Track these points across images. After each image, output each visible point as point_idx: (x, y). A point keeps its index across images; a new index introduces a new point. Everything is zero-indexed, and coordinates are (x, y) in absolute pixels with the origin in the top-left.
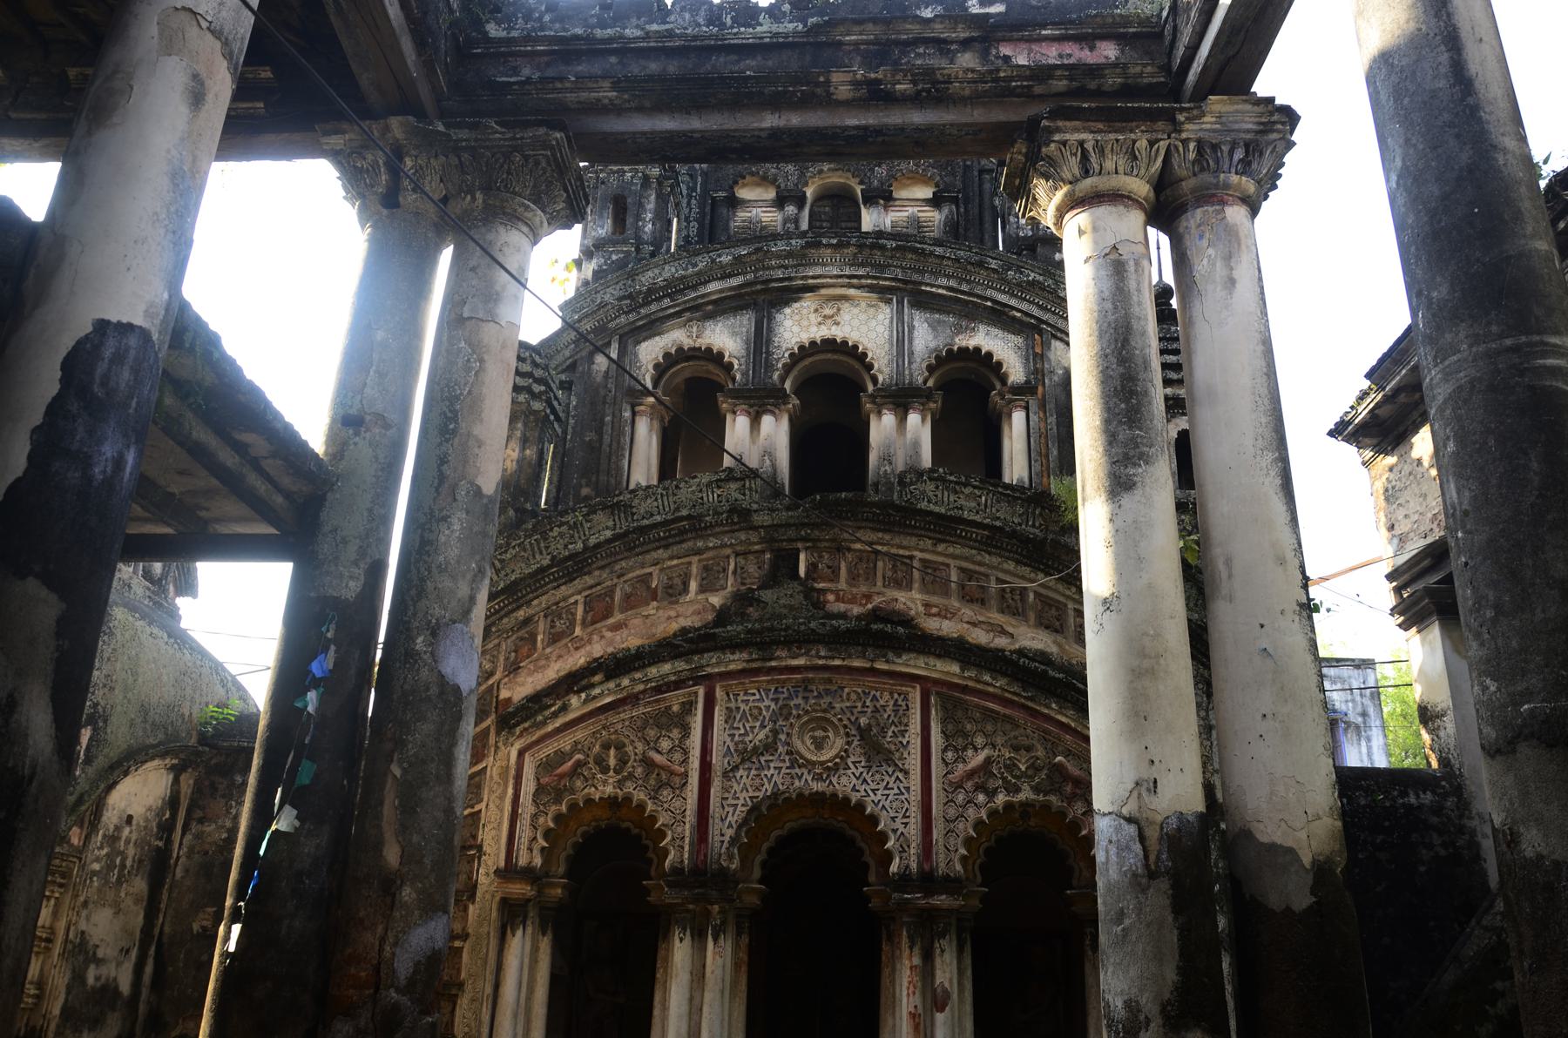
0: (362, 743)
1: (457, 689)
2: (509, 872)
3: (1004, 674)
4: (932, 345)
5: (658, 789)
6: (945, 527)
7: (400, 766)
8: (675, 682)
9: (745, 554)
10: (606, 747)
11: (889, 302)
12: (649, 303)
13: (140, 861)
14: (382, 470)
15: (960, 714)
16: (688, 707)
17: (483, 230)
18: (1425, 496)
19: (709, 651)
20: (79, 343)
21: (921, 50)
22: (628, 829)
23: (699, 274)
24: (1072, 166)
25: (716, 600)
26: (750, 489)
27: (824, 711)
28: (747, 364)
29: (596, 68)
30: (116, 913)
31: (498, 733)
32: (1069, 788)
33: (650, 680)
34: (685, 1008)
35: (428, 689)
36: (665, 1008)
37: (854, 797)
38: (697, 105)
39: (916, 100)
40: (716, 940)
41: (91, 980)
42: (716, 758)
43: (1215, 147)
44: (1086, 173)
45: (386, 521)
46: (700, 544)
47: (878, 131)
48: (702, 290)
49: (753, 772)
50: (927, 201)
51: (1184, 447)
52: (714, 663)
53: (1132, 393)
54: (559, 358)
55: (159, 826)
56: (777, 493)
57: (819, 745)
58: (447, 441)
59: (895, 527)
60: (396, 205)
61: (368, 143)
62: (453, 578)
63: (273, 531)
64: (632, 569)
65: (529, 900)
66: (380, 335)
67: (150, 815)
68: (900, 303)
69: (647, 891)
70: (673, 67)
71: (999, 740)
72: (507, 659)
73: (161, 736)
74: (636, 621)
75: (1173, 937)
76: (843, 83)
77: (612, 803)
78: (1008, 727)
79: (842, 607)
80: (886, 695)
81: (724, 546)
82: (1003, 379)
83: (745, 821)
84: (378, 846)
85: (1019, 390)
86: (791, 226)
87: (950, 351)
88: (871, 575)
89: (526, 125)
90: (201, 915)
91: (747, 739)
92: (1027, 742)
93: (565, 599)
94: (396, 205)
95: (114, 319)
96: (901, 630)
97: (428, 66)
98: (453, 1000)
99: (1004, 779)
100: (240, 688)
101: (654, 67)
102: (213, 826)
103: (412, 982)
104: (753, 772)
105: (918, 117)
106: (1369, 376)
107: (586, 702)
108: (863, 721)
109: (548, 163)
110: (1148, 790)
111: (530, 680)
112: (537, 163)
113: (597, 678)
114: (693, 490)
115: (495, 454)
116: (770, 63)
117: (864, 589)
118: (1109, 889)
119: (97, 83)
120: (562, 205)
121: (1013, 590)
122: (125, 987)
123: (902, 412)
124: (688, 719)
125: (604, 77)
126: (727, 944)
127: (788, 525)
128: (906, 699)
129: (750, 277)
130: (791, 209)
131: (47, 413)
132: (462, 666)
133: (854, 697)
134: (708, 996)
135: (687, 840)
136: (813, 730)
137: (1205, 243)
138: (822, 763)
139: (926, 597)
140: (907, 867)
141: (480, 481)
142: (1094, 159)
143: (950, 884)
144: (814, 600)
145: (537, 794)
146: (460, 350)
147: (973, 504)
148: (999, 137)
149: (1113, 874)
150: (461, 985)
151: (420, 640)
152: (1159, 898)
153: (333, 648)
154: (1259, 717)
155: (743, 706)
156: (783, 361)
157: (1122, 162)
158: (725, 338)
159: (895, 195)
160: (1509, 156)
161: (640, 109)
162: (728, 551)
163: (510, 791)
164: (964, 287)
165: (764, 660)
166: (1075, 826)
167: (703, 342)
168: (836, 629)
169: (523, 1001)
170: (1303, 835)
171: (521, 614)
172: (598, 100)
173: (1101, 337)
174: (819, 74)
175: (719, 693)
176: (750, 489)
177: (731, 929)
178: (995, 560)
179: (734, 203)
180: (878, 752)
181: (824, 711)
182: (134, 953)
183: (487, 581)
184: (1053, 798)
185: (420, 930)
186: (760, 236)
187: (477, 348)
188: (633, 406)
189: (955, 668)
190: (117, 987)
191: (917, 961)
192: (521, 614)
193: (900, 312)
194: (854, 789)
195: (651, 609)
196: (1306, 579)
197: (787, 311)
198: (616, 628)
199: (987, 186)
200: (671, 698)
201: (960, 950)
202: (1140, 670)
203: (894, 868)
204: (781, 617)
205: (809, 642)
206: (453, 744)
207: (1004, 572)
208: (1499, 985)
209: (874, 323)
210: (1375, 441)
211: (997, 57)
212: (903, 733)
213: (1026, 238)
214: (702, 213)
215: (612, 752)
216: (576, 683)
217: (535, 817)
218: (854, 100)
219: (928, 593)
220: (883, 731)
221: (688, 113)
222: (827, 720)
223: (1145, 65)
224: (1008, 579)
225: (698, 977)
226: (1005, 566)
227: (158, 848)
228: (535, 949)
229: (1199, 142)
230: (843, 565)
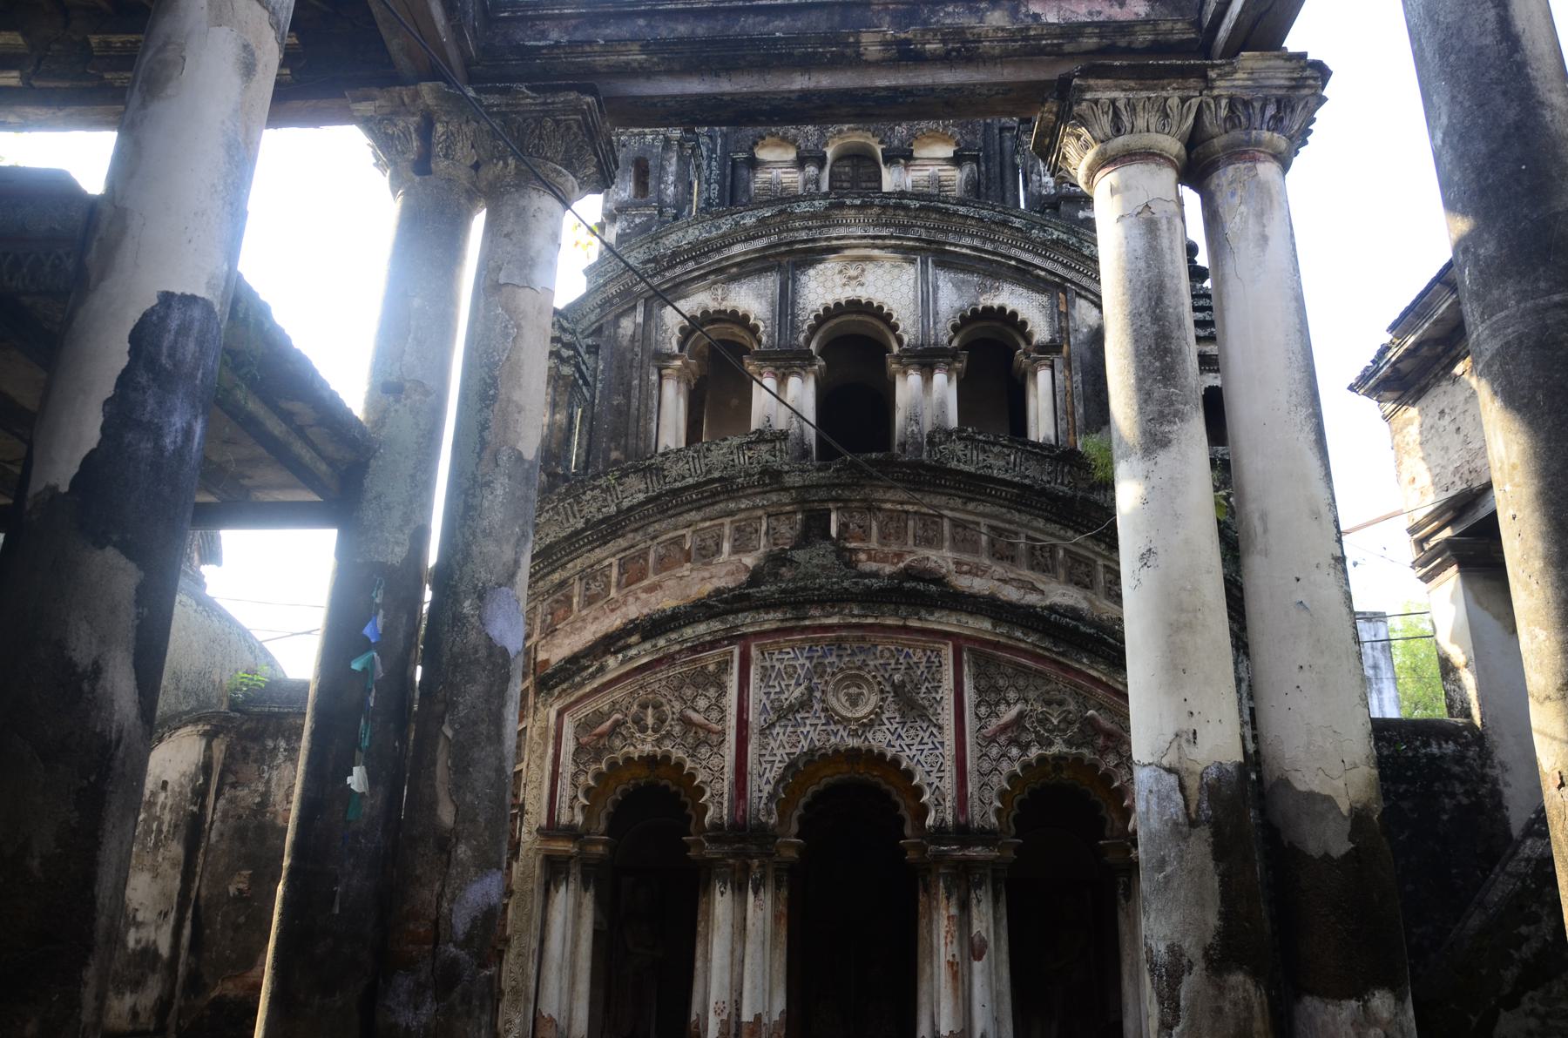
0: (411, 707)
1: (504, 651)
2: (551, 830)
3: (1036, 630)
4: (957, 305)
5: (695, 748)
6: (975, 486)
7: (452, 727)
8: (710, 642)
9: (776, 515)
10: (644, 706)
11: (913, 262)
12: (674, 267)
13: (176, 826)
14: (423, 436)
15: (992, 669)
16: (724, 666)
17: (516, 196)
18: (1446, 449)
19: (743, 610)
20: (145, 314)
21: (950, 9)
22: (666, 787)
23: (723, 236)
24: (1106, 122)
25: (749, 561)
26: (781, 451)
27: (859, 668)
28: (773, 326)
29: (624, 30)
30: (155, 877)
31: (537, 694)
32: (1100, 741)
33: (685, 641)
34: (727, 960)
35: (476, 652)
36: (707, 960)
37: (890, 753)
38: (727, 66)
39: (946, 60)
40: (756, 893)
41: (131, 943)
42: (753, 716)
43: (1247, 104)
44: (1118, 130)
45: (428, 486)
46: (732, 505)
47: (908, 92)
48: (727, 253)
49: (790, 729)
50: (948, 160)
51: (1214, 404)
52: (748, 622)
53: (1167, 351)
54: (585, 323)
55: (194, 791)
56: (805, 453)
57: (854, 702)
58: (487, 407)
59: (951, 487)
60: (429, 172)
61: (400, 109)
62: (498, 541)
63: (317, 499)
64: (666, 532)
65: (571, 857)
66: (417, 302)
67: (185, 781)
68: (924, 263)
69: (687, 847)
70: (702, 29)
71: (1032, 695)
72: (543, 621)
73: (193, 703)
74: (670, 583)
75: (1214, 883)
76: (873, 44)
77: (650, 761)
78: (1039, 682)
79: (874, 566)
80: (919, 653)
81: (755, 507)
82: (1028, 337)
83: (782, 778)
84: (432, 806)
85: (1044, 349)
86: (812, 187)
87: (974, 311)
88: (900, 534)
89: (557, 89)
90: (237, 878)
91: (783, 697)
92: (1059, 697)
93: (599, 562)
94: (429, 172)
95: (178, 291)
96: (933, 588)
97: (457, 30)
98: (500, 955)
99: (1037, 733)
100: (267, 654)
101: (682, 29)
102: (246, 791)
103: (469, 937)
104: (790, 729)
105: (949, 77)
106: (1392, 328)
107: (622, 663)
108: (897, 678)
109: (580, 127)
110: (1188, 741)
111: (567, 641)
112: (569, 128)
113: (634, 639)
114: (722, 454)
115: (532, 419)
116: (799, 24)
117: (895, 548)
118: (1151, 837)
119: (149, 54)
120: (593, 170)
121: (1042, 548)
122: (164, 949)
123: (927, 371)
124: (724, 678)
125: (633, 40)
126: (767, 897)
127: (818, 486)
128: (938, 655)
129: (774, 239)
130: (811, 170)
131: (117, 386)
132: (508, 626)
133: (887, 654)
134: (749, 948)
135: (726, 796)
136: (848, 687)
137: (1237, 200)
138: (857, 720)
139: (956, 555)
140: (943, 820)
141: (521, 446)
142: (1125, 117)
143: (985, 836)
144: (846, 558)
145: (577, 753)
146: (497, 316)
147: (1002, 463)
148: (1023, 98)
149: (1155, 823)
150: (507, 941)
151: (467, 603)
152: (1200, 846)
153: (381, 612)
154: (1296, 669)
155: (778, 665)
156: (809, 322)
157: (1154, 120)
158: (751, 300)
159: (915, 154)
160: (1556, 113)
161: (670, 72)
162: (760, 513)
163: (550, 751)
164: (988, 247)
165: (798, 619)
166: (1108, 778)
167: (728, 305)
168: (869, 588)
169: (567, 954)
170: (1340, 783)
171: (557, 577)
172: (628, 63)
173: (1133, 297)
174: (849, 35)
175: (754, 652)
176: (781, 451)
177: (770, 883)
178: (1025, 518)
179: (754, 164)
180: (912, 707)
181: (859, 668)
182: (172, 917)
183: (530, 545)
184: (1085, 751)
185: (476, 887)
186: (782, 199)
187: (512, 312)
188: (660, 370)
189: (987, 625)
190: (156, 950)
191: (953, 911)
192: (557, 577)
193: (924, 272)
194: (889, 745)
195: (685, 569)
196: (1339, 532)
197: (812, 272)
198: (651, 589)
199: (1008, 144)
200: (706, 658)
201: (996, 900)
202: (1177, 625)
203: (930, 821)
204: (814, 576)
205: (842, 600)
206: (502, 705)
207: (1033, 529)
208: (1524, 930)
209: (898, 284)
210: (1396, 395)
211: (1027, 15)
212: (936, 689)
213: (1048, 196)
214: (723, 175)
215: (650, 711)
216: (613, 644)
217: (575, 776)
218: (884, 60)
219: (958, 551)
220: (917, 687)
221: (717, 75)
222: (862, 677)
223: (1175, 22)
224: (1038, 536)
225: (740, 929)
226: (1035, 524)
227: (193, 813)
228: (578, 905)
229: (1232, 101)
230: (874, 524)
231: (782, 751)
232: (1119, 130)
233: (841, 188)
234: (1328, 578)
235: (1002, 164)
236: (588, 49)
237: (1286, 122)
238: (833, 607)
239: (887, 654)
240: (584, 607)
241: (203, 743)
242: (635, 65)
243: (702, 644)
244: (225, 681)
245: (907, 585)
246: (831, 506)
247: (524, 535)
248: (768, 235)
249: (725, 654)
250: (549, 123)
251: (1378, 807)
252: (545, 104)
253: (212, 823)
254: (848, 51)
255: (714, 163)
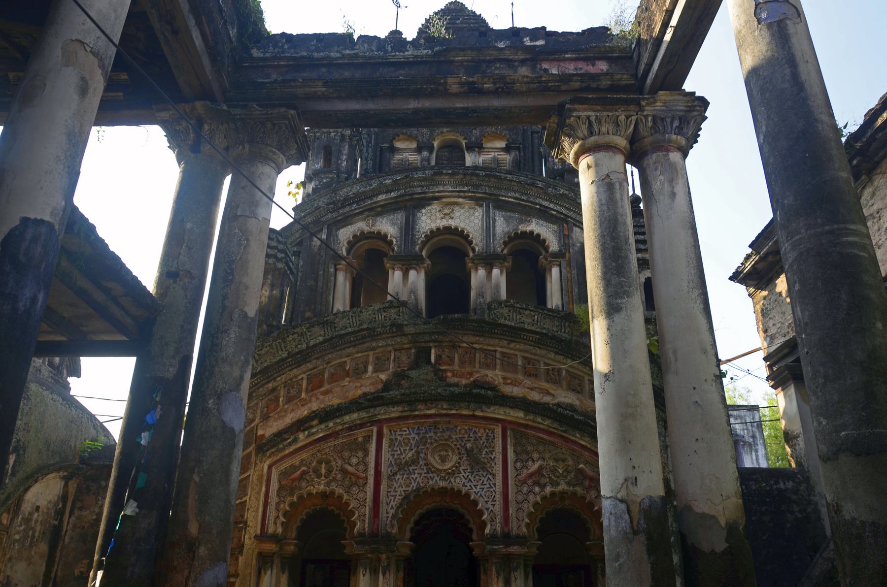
2: (262, 537)
3: (549, 418)
4: (506, 230)
6: (515, 333)
8: (360, 424)
10: (320, 462)
11: (481, 206)
13: (44, 533)
16: (367, 439)
18: (784, 313)
19: (379, 406)
21: (498, 65)
22: (333, 511)
23: (373, 190)
24: (583, 130)
25: (383, 377)
26: (403, 313)
27: (446, 440)
28: (401, 241)
30: (29, 564)
31: (256, 455)
32: (587, 483)
33: (345, 423)
39: (495, 93)
40: (384, 575)
43: (663, 120)
44: (591, 134)
46: (374, 344)
47: (474, 111)
48: (375, 200)
49: (405, 476)
50: (502, 149)
51: (648, 287)
52: (382, 413)
54: (293, 238)
56: (417, 313)
57: (443, 460)
58: (227, 286)
63: (124, 338)
68: (488, 206)
69: (344, 547)
70: (358, 74)
71: (547, 456)
72: (262, 412)
73: (57, 459)
74: (337, 389)
75: (647, 568)
76: (454, 83)
77: (324, 495)
79: (456, 380)
80: (482, 431)
81: (388, 345)
82: (546, 249)
83: (401, 505)
85: (555, 255)
86: (426, 163)
87: (516, 234)
91: (402, 457)
93: (296, 377)
94: (199, 151)
96: (490, 393)
99: (550, 478)
101: (347, 74)
102: (88, 512)
104: (405, 476)
105: (496, 103)
107: (308, 436)
108: (469, 445)
110: (632, 483)
111: (275, 424)
113: (315, 422)
114: (369, 313)
115: (255, 294)
116: (413, 72)
117: (468, 369)
121: (553, 369)
124: (367, 445)
126: (391, 577)
127: (424, 333)
128: (493, 432)
129: (402, 192)
130: (425, 154)
132: (236, 417)
133: (463, 431)
135: (367, 517)
136: (440, 451)
137: (658, 173)
138: (445, 470)
139: (503, 374)
141: (246, 309)
143: (520, 540)
144: (440, 376)
145: (279, 491)
147: (530, 320)
148: (543, 113)
149: (613, 532)
151: (211, 401)
152: (640, 545)
153: (159, 406)
154: (694, 440)
155: (399, 438)
158: (388, 226)
159: (484, 146)
161: (339, 98)
162: (390, 348)
163: (264, 489)
164: (524, 197)
166: (591, 505)
167: (375, 229)
170: (720, 508)
171: (270, 385)
172: (315, 92)
175: (385, 430)
176: (403, 313)
178: (543, 352)
179: (393, 150)
180: (477, 463)
181: (446, 440)
183: (250, 367)
186: (408, 168)
189: (521, 414)
192: (270, 385)
193: (488, 212)
194: (464, 485)
195: (346, 382)
197: (424, 211)
198: (325, 393)
199: (536, 141)
201: (526, 578)
202: (625, 413)
203: (487, 531)
205: (436, 400)
206: (230, 462)
207: (548, 358)
209: (473, 218)
210: (755, 283)
211: (541, 69)
212: (492, 452)
215: (323, 465)
217: (278, 504)
220: (480, 451)
222: (448, 445)
223: (623, 74)
226: (549, 355)
227: (55, 525)
231: (400, 489)
232: (592, 133)
233: (442, 164)
234: (714, 388)
235: (533, 152)
236: (293, 84)
237: (685, 130)
238: (431, 404)
239: (463, 431)
240: (286, 403)
241: (63, 483)
242: (320, 93)
243: (355, 426)
244: (78, 446)
245: (475, 391)
246: (431, 345)
247: (247, 361)
248: (399, 190)
249: (368, 431)
250: (269, 125)
251: (742, 522)
252: (267, 114)
253: (67, 531)
254: (441, 88)
255: (370, 149)
